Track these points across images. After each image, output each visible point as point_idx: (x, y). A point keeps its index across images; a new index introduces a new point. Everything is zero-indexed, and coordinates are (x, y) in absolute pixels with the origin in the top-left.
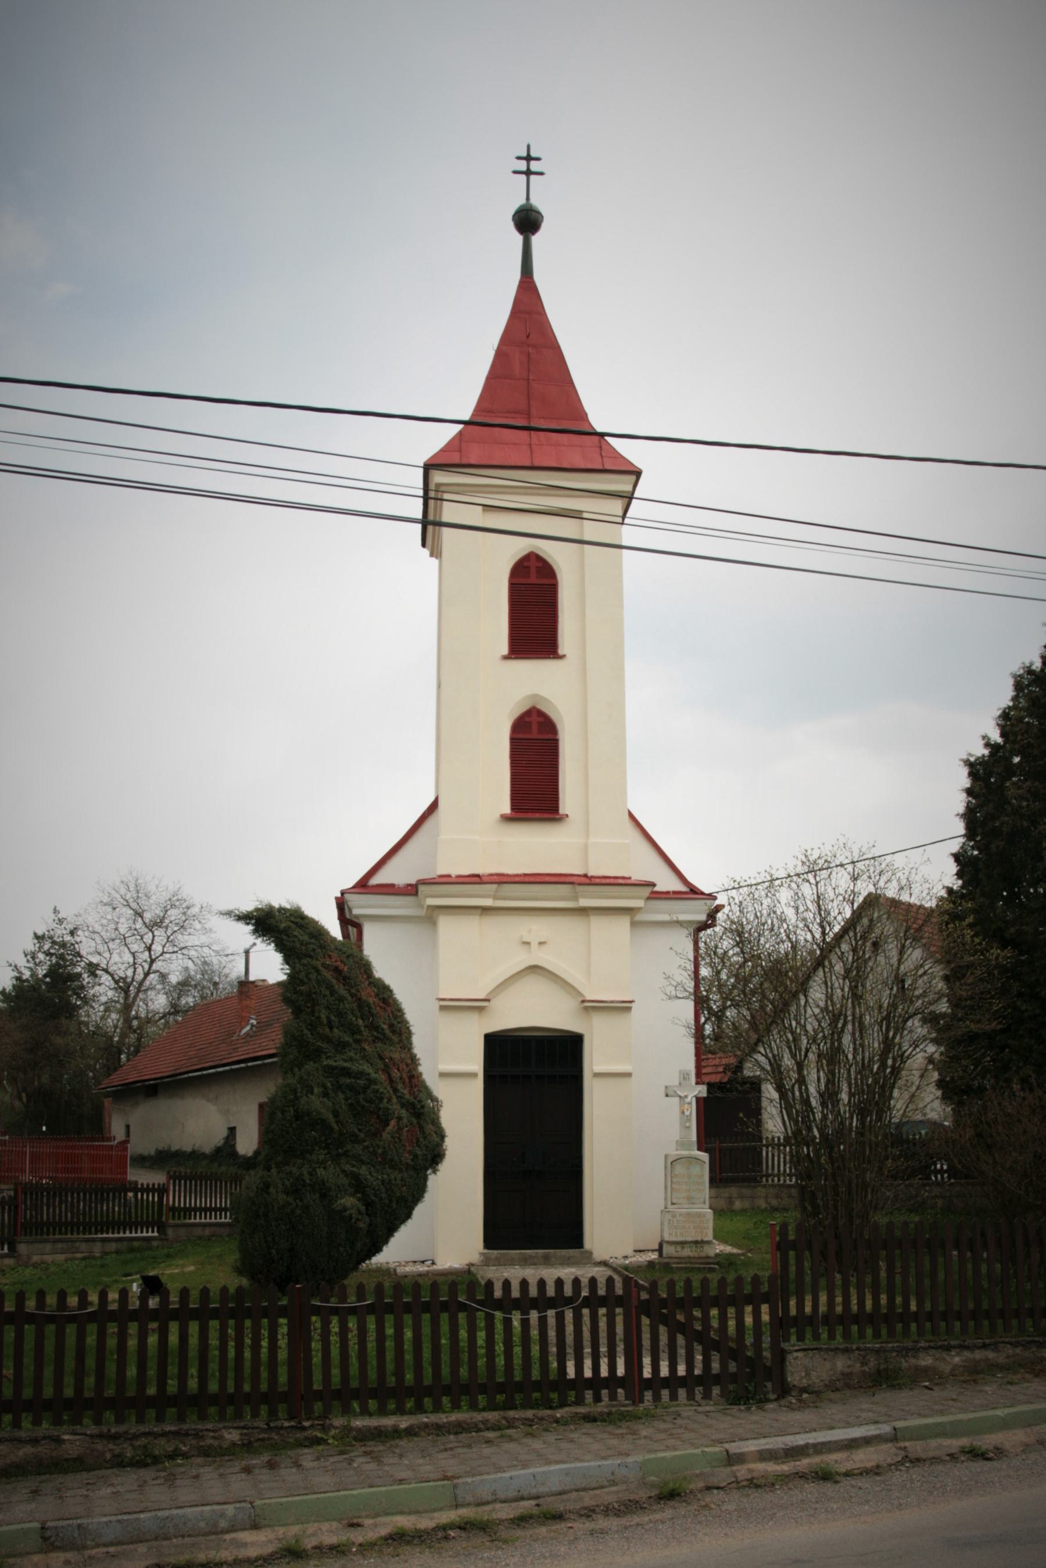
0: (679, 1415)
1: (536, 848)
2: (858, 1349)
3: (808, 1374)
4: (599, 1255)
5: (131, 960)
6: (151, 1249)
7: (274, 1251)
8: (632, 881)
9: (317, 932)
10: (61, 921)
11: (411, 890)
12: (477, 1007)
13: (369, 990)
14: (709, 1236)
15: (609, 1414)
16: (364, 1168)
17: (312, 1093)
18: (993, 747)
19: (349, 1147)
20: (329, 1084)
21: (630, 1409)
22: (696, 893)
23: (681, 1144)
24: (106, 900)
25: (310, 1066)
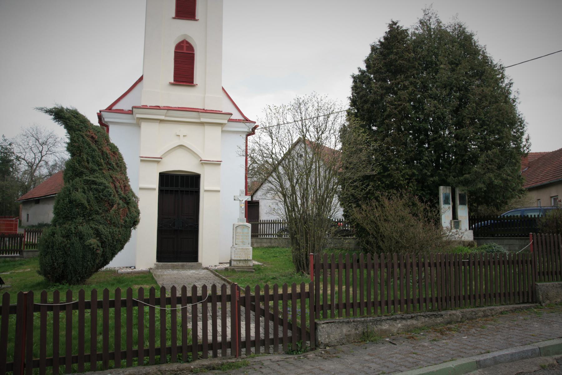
0: (263, 364)
1: (183, 97)
2: (354, 321)
3: (329, 336)
4: (204, 265)
5: (34, 156)
6: (15, 261)
7: (56, 264)
8: (223, 112)
9: (84, 121)
10: (5, 140)
11: (131, 112)
12: (157, 161)
13: (107, 147)
14: (251, 258)
15: (222, 364)
16: (101, 226)
17: (78, 191)
18: (362, 72)
19: (94, 216)
20: (86, 188)
21: (233, 360)
22: (247, 120)
23: (240, 220)
24: (24, 134)
25: (77, 179)
